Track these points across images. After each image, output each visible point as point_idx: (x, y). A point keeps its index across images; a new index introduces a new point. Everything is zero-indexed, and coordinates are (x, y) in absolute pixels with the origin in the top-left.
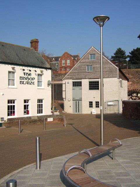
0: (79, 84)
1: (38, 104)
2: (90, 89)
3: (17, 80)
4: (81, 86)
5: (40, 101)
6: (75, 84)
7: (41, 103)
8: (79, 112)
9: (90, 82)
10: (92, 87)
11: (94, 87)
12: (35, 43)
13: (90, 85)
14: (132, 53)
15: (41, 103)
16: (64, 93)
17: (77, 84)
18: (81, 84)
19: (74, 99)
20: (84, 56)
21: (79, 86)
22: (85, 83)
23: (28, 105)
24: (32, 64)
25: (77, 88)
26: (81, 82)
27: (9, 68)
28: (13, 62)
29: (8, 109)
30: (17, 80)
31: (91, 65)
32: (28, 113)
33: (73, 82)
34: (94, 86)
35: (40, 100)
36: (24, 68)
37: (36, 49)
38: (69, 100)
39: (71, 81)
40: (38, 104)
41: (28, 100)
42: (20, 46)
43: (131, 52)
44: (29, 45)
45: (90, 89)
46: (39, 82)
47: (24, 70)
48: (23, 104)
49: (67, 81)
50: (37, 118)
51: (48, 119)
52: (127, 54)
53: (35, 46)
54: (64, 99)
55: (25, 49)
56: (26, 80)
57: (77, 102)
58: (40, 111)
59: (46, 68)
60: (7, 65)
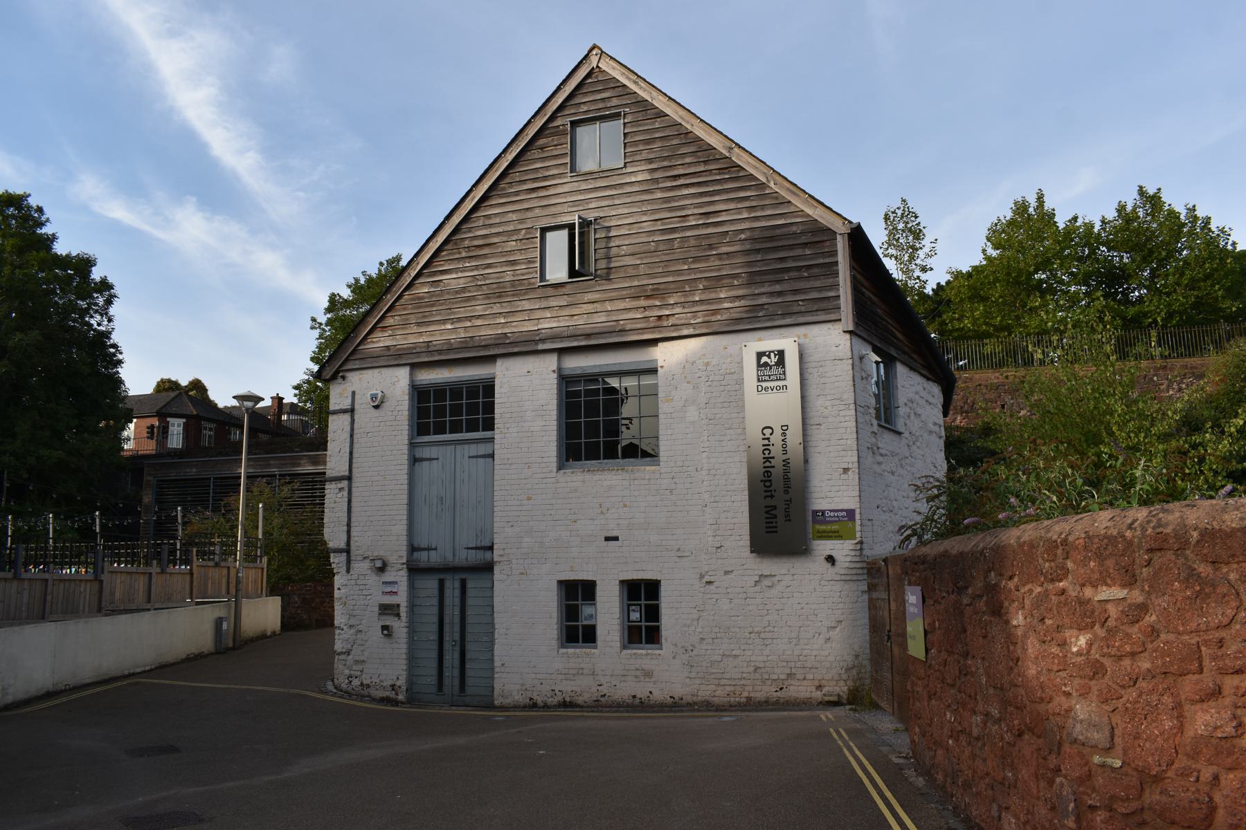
0: (473, 409)
4: (489, 425)
6: (473, 409)
9: (566, 380)
16: (333, 496)
18: (490, 408)
21: (472, 427)
25: (450, 455)
26: (488, 388)
54: (337, 561)
57: (453, 579)
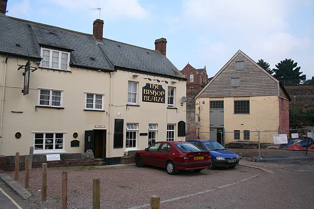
1: (173, 131)
4: (223, 107)
6: (220, 105)
7: (172, 130)
9: (235, 102)
10: (245, 109)
11: (242, 109)
12: (161, 44)
13: (249, 109)
14: (280, 66)
15: (172, 130)
17: (217, 105)
19: (211, 126)
20: (233, 59)
21: (220, 107)
22: (229, 104)
24: (161, 73)
25: (217, 111)
27: (129, 75)
29: (135, 141)
31: (238, 77)
33: (211, 102)
34: (242, 107)
35: (170, 126)
36: (149, 77)
37: (163, 53)
39: (207, 101)
40: (173, 131)
43: (277, 65)
44: (153, 48)
46: (171, 101)
49: (202, 100)
50: (118, 71)
53: (162, 48)
55: (148, 51)
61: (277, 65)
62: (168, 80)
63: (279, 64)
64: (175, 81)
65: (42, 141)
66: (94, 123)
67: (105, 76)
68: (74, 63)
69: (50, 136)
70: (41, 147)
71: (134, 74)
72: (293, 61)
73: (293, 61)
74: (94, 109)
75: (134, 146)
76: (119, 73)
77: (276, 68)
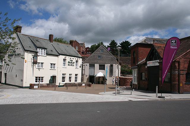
2: (99, 69)
3: (67, 63)
5: (76, 75)
8: (109, 88)
22: (97, 66)
23: (71, 77)
25: (92, 69)
27: (63, 57)
28: (73, 55)
30: (67, 63)
32: (70, 81)
38: (87, 75)
41: (65, 74)
42: (182, 39)
43: (121, 43)
45: (99, 69)
47: (70, 58)
48: (62, 76)
51: (34, 86)
52: (119, 44)
56: (71, 63)
58: (76, 81)
59: (79, 57)
60: (63, 56)
61: (121, 43)
62: (76, 58)
63: (122, 43)
64: (78, 58)
65: (37, 80)
66: (53, 73)
67: (56, 58)
68: (48, 53)
69: (39, 78)
70: (37, 82)
71: (65, 56)
72: (131, 44)
73: (131, 44)
74: (53, 69)
75: (64, 82)
76: (61, 56)
77: (109, 45)
